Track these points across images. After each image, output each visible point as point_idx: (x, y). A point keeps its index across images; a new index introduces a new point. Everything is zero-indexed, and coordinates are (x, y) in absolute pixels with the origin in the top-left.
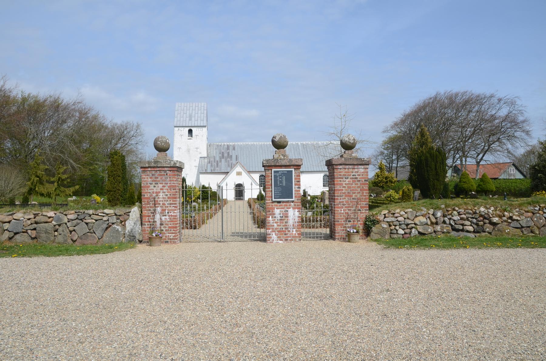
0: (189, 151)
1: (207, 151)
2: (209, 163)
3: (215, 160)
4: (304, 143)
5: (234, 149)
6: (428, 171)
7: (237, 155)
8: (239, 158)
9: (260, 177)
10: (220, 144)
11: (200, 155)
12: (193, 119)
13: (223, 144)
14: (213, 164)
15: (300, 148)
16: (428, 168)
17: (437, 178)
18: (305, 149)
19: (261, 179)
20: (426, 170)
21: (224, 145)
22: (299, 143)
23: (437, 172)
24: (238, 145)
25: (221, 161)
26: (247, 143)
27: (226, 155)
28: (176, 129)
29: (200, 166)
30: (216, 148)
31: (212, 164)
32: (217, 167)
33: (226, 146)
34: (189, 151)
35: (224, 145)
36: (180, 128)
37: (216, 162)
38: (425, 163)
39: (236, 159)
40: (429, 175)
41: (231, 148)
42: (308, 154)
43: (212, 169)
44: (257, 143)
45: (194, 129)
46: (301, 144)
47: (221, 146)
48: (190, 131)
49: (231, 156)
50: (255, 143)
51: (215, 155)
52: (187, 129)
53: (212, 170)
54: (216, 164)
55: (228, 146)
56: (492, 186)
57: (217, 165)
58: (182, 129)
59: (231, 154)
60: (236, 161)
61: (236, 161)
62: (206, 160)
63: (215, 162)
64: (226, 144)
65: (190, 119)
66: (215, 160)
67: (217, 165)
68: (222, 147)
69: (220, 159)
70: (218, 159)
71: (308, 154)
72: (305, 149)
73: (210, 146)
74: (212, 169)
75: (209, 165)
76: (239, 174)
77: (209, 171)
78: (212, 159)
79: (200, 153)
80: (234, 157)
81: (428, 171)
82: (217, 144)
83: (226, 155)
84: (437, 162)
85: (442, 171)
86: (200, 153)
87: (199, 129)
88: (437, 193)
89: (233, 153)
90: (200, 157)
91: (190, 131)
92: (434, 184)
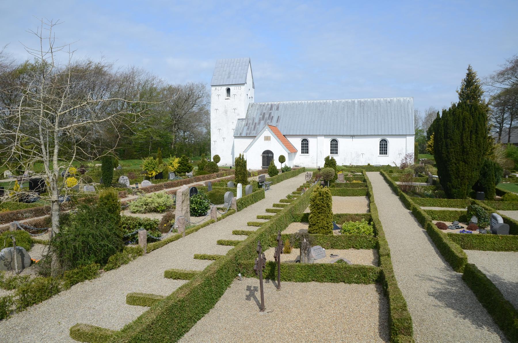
0: (226, 112)
1: (247, 113)
2: (246, 125)
3: (253, 122)
4: (362, 100)
5: (278, 109)
6: (447, 146)
7: (279, 116)
8: (281, 119)
9: (302, 141)
10: (264, 103)
11: (239, 116)
12: (232, 76)
13: (267, 103)
14: (250, 127)
15: (356, 106)
16: (448, 140)
17: (465, 157)
18: (362, 107)
19: (304, 144)
20: (444, 143)
21: (268, 105)
22: (356, 101)
23: (464, 148)
24: (283, 104)
25: (259, 123)
26: (294, 102)
27: (267, 116)
28: (213, 88)
29: (237, 130)
30: (258, 109)
31: (249, 127)
32: (254, 130)
33: (270, 106)
34: (226, 112)
35: (268, 105)
36: (217, 88)
37: (254, 124)
38: (443, 131)
39: (277, 121)
40: (448, 152)
41: (274, 108)
42: (364, 113)
43: (248, 132)
44: (306, 101)
45: (232, 88)
46: (358, 101)
47: (264, 106)
48: (228, 90)
49: (273, 117)
50: (303, 102)
51: (255, 116)
52: (224, 88)
53: (247, 134)
54: (253, 127)
55: (272, 105)
56: (377, 260)
57: (255, 127)
58: (219, 88)
59: (272, 115)
60: (277, 122)
61: (277, 122)
62: (244, 123)
63: (253, 124)
64: (270, 103)
65: (229, 77)
66: (253, 122)
67: (255, 127)
68: (264, 108)
69: (260, 120)
70: (257, 121)
71: (364, 113)
72: (362, 107)
73: (252, 106)
74: (248, 132)
75: (246, 128)
76: (267, 138)
77: (244, 135)
78: (250, 121)
79: (238, 115)
80: (275, 119)
81: (447, 146)
82: (260, 103)
83: (267, 116)
84: (464, 129)
85: (474, 145)
86: (238, 115)
87: (237, 87)
88: (465, 185)
89: (275, 114)
90: (238, 119)
91: (228, 90)
92: (457, 169)
